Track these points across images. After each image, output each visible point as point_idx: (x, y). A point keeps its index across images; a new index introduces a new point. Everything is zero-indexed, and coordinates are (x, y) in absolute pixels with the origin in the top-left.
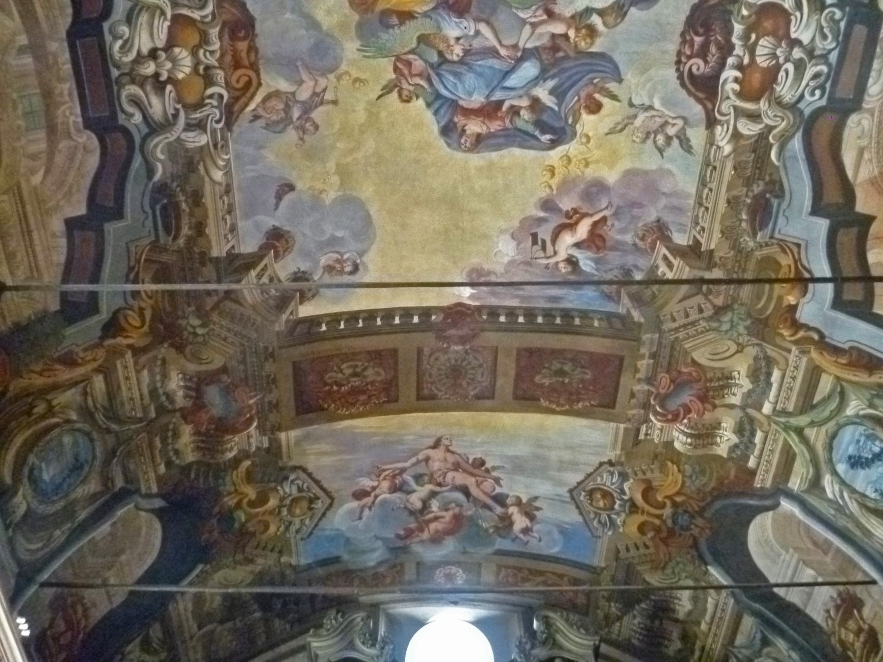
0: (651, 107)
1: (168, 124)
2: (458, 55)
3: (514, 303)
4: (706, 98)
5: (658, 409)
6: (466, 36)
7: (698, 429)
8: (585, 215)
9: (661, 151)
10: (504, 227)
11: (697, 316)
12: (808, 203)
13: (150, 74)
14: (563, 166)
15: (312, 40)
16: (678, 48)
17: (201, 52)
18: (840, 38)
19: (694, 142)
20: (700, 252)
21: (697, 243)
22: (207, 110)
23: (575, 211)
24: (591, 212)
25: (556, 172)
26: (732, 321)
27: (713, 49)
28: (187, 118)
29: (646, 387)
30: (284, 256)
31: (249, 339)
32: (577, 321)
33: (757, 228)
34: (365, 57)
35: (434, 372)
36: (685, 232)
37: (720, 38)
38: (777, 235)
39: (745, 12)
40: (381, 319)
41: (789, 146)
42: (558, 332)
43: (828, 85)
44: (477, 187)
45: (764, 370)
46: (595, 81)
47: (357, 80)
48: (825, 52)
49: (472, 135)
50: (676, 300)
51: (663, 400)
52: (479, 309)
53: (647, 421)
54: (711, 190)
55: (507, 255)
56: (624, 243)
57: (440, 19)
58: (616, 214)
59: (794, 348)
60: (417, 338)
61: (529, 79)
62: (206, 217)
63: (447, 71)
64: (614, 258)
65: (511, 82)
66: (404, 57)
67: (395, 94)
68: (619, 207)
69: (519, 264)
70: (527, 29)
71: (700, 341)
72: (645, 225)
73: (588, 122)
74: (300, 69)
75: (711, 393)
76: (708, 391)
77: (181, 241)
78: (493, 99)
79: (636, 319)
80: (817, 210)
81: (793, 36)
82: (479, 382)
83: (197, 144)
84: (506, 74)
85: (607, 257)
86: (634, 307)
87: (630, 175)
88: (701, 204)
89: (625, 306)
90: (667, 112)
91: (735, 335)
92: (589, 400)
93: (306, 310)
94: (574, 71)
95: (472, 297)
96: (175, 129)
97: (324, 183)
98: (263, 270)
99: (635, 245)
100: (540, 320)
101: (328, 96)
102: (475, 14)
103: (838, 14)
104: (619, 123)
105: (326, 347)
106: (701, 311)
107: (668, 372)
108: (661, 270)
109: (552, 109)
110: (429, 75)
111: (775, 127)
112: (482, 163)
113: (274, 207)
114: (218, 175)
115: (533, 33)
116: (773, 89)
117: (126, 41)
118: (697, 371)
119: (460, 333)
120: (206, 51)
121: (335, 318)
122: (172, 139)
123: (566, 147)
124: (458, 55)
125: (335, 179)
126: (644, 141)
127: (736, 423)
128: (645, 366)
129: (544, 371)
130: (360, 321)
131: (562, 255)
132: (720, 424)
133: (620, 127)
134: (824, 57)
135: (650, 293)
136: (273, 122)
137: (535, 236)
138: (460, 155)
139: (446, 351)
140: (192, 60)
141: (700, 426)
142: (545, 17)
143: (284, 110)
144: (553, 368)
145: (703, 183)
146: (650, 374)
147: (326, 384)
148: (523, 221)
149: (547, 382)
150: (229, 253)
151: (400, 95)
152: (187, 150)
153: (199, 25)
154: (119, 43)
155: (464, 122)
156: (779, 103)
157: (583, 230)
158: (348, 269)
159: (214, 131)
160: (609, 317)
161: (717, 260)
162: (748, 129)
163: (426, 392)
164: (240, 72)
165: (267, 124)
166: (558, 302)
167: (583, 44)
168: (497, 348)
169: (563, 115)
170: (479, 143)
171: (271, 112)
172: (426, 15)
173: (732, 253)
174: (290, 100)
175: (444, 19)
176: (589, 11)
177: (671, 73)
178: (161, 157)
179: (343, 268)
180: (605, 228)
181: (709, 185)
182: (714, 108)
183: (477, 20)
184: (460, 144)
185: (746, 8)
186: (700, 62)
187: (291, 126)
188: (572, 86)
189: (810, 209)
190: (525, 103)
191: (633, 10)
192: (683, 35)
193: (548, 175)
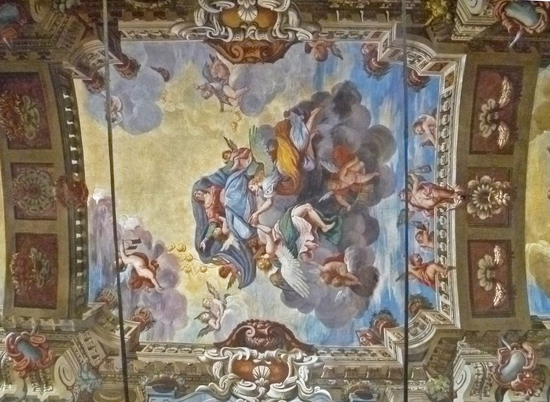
0: (225, 308)
2: (252, 188)
3: (90, 230)
4: (232, 341)
5: (17, 338)
6: (263, 193)
7: (4, 369)
8: (155, 274)
9: (199, 317)
10: (144, 221)
11: (90, 356)
14: (186, 257)
15: (260, 98)
16: (260, 320)
17: (254, 28)
19: (205, 336)
21: (140, 349)
22: (218, 27)
23: (157, 267)
24: (157, 277)
25: (182, 253)
26: (89, 379)
27: (261, 340)
28: (213, 14)
29: (33, 327)
30: (118, 71)
31: (55, 42)
32: (79, 274)
33: (155, 385)
34: (250, 130)
35: (35, 175)
36: (148, 339)
38: (150, 398)
39: (282, 356)
40: (73, 138)
41: (208, 396)
42: (71, 263)
44: (170, 202)
46: (239, 272)
47: (236, 124)
49: (203, 198)
50: (102, 341)
51: (25, 341)
52: (84, 205)
53: (7, 331)
54: (177, 352)
55: (125, 224)
56: (137, 301)
58: (156, 293)
60: (60, 162)
61: (239, 232)
65: (237, 221)
66: (250, 154)
67: (228, 149)
68: (161, 294)
70: (268, 229)
71: (72, 360)
72: (150, 313)
73: (214, 270)
74: (243, 89)
75: (34, 373)
76: (35, 371)
78: (226, 210)
81: (271, 386)
82: (28, 208)
83: (196, 19)
84: (241, 218)
85: (127, 290)
86: (93, 312)
87: (182, 299)
88: (167, 347)
89: (93, 306)
90: (223, 318)
91: (80, 383)
92: (20, 288)
93: (79, 85)
94: (245, 260)
95: (93, 201)
96: (206, 5)
97: (170, 101)
99: (137, 308)
100: (79, 249)
101: (226, 106)
102: (276, 197)
104: (214, 289)
105: (51, 98)
106: (94, 357)
107: (47, 341)
109: (221, 247)
110: (240, 170)
111: (218, 385)
112: (185, 205)
114: (175, 31)
115: (266, 233)
116: (240, 380)
118: (49, 361)
119: (66, 194)
120: (255, 31)
121: (73, 105)
123: (198, 258)
124: (252, 188)
125: (172, 109)
126: (204, 306)
127: (13, 395)
128: (50, 324)
129: (40, 254)
130: (72, 123)
131: (126, 260)
132: (11, 383)
133: (212, 290)
135: (104, 322)
136: (210, 70)
137: (139, 241)
138: (190, 190)
139: (51, 184)
140: (249, 21)
141: (7, 370)
142: (275, 240)
144: (43, 261)
145: (180, 346)
146: (44, 329)
147: (21, 96)
149: (32, 256)
150: (120, 33)
151: (227, 152)
152: (192, 12)
153: (270, 28)
155: (211, 193)
156: (233, 385)
157: (145, 273)
159: (204, 31)
160: (85, 296)
162: (216, 369)
163: (18, 170)
164: (242, 52)
165: (208, 66)
166: (93, 259)
167: (261, 263)
168: (56, 220)
169: (217, 255)
170: (199, 202)
171: (216, 69)
172: (275, 168)
173: (137, 372)
174: (224, 82)
175: (273, 179)
176: (279, 265)
177: (246, 318)
180: (147, 287)
181: (179, 350)
183: (272, 199)
184: (197, 190)
185: (284, 356)
187: (207, 82)
188: (235, 258)
190: (225, 230)
191: (281, 291)
192: (268, 322)
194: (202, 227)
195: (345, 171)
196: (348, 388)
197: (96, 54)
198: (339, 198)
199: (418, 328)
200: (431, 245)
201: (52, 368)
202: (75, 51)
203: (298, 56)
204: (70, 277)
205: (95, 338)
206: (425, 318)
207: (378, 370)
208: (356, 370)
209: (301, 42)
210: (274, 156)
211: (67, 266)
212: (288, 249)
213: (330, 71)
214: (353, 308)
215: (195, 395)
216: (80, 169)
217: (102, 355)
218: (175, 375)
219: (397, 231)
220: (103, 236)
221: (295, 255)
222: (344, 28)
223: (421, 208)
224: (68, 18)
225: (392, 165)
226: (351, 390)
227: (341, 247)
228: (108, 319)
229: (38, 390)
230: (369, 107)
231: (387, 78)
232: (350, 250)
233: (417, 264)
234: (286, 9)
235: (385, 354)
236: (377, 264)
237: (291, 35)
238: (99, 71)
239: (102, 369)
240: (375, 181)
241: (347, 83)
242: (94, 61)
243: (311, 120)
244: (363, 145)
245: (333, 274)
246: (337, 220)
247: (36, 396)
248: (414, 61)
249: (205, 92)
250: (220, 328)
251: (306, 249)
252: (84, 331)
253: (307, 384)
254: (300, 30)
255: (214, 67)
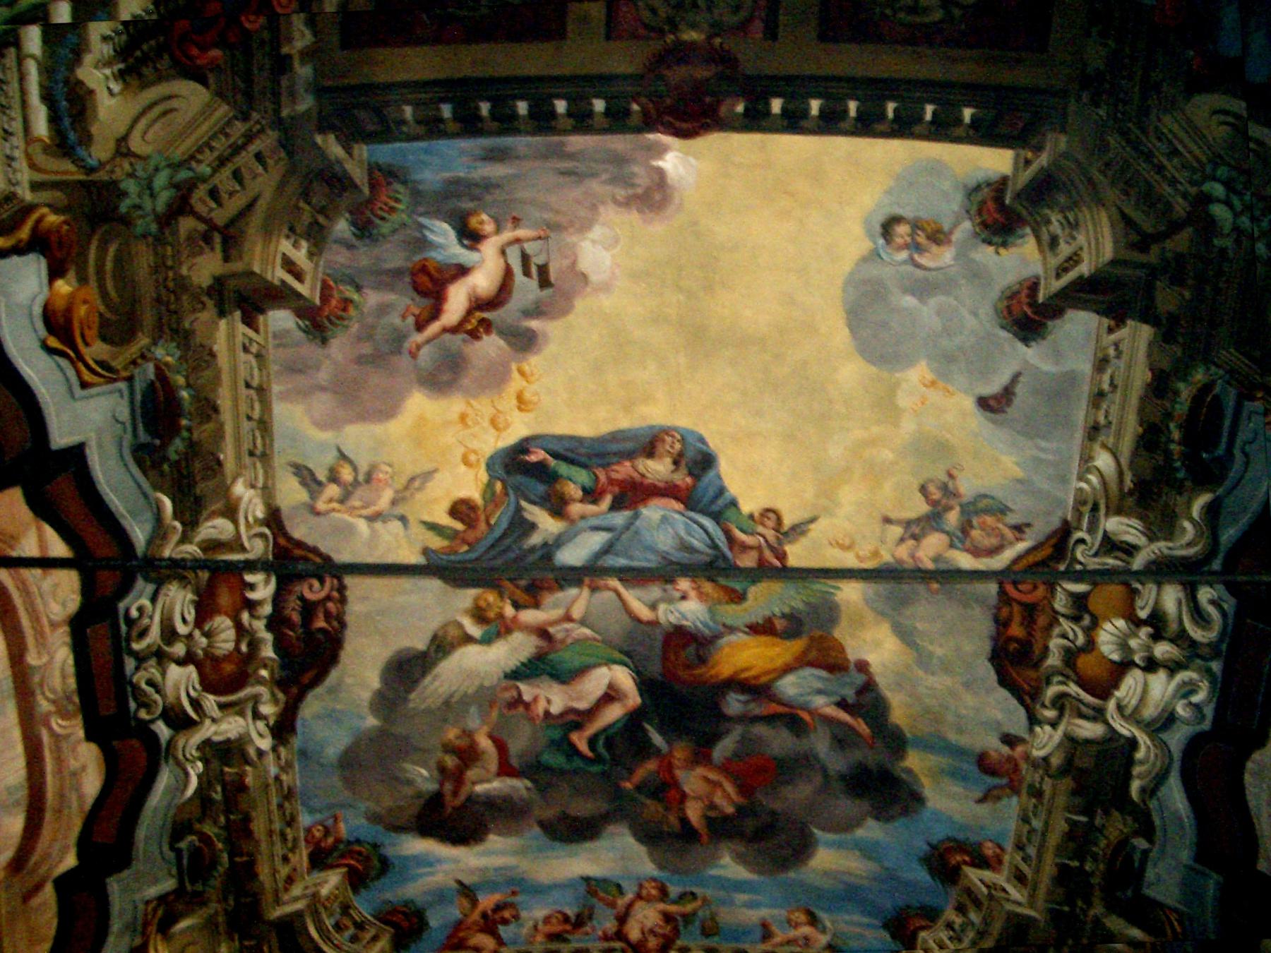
1: (1161, 570)
3: (577, 142)
6: (670, 601)
8: (454, 330)
9: (343, 456)
10: (602, 297)
12: (94, 459)
13: (1165, 643)
15: (908, 612)
18: (129, 689)
20: (240, 307)
21: (249, 321)
23: (474, 335)
24: (447, 336)
25: (514, 402)
26: (153, 196)
27: (296, 617)
31: (1124, 133)
32: (446, 111)
33: (158, 385)
36: (275, 336)
37: (291, 633)
39: (264, 673)
40: (846, 111)
41: (148, 527)
42: (479, 81)
43: (124, 628)
45: (67, 122)
47: (849, 548)
48: (145, 665)
49: (661, 457)
50: (262, 205)
52: (649, 124)
54: (249, 418)
56: (379, 286)
57: (711, 624)
58: (398, 338)
59: (28, 196)
62: (1143, 399)
63: (702, 553)
64: (395, 257)
65: (598, 540)
67: (788, 522)
68: (398, 351)
69: (571, 223)
70: (577, 613)
72: (347, 327)
77: (1199, 376)
79: (331, 137)
80: (77, 453)
83: (1125, 520)
84: (607, 549)
86: (339, 162)
87: (388, 411)
90: (347, 517)
95: (661, 151)
96: (1153, 556)
98: (1066, 270)
99: (358, 288)
100: (522, 107)
101: (897, 531)
102: (658, 631)
103: (143, 714)
104: (419, 489)
106: (214, 194)
108: (304, 251)
110: (731, 549)
113: (1021, 379)
117: (1185, 696)
118: (191, 58)
121: (942, 130)
122: (1162, 544)
125: (903, 401)
128: (297, 35)
130: (890, 114)
131: (489, 249)
133: (417, 484)
134: (141, 659)
137: (545, 282)
138: (683, 421)
139: (717, 28)
142: (551, 630)
143: (972, 527)
145: (264, 425)
148: (565, 311)
150: (1120, 321)
154: (1196, 699)
157: (457, 300)
158: (902, 229)
159: (1092, 529)
160: (386, 131)
161: (210, 303)
164: (1027, 599)
169: (511, 492)
170: (650, 444)
171: (993, 529)
172: (731, 629)
173: (187, 325)
175: (706, 625)
176: (487, 641)
178: (1187, 524)
179: (913, 235)
181: (254, 424)
182: (275, 539)
183: (654, 623)
184: (683, 440)
185: (263, 677)
186: (309, 595)
187: (965, 500)
188: (504, 535)
189: (88, 451)
190: (576, 509)
192: (343, 625)
193: (527, 395)
194: (583, 451)
195: (713, 776)
196: (209, 829)
197: (1074, 238)
198: (651, 765)
199: (351, 931)
200: (540, 938)
201: (172, 72)
202: (1091, 181)
203: (1000, 716)
204: (436, 83)
205: (264, 183)
206: (375, 939)
207: (256, 875)
208: (249, 834)
209: (1031, 730)
210: (762, 629)
211: (467, 71)
212: (530, 661)
213: (954, 774)
214: (388, 802)
215: (145, 495)
216: (756, 121)
217: (221, 216)
218: (189, 430)
219: (570, 876)
220: (561, 179)
221: (515, 675)
222: (1046, 824)
223: (622, 919)
224: (1185, 196)
225: (722, 867)
226: (204, 838)
227: (533, 769)
228: (322, 211)
229: (107, 50)
230: (860, 833)
231: (921, 875)
232: (528, 789)
233: (497, 917)
234: (1111, 721)
235: (290, 880)
236: (494, 841)
237: (1050, 714)
238: (1028, 230)
239: (187, 224)
240: (687, 834)
241: (917, 799)
242: (1055, 227)
243: (844, 716)
244: (773, 813)
245: (468, 755)
246: (598, 759)
247: (90, 51)
248: (953, 929)
249: (938, 488)
250: (318, 514)
251: (527, 697)
252: (284, 147)
253: (207, 743)
254: (1058, 735)
255: (1000, 526)
